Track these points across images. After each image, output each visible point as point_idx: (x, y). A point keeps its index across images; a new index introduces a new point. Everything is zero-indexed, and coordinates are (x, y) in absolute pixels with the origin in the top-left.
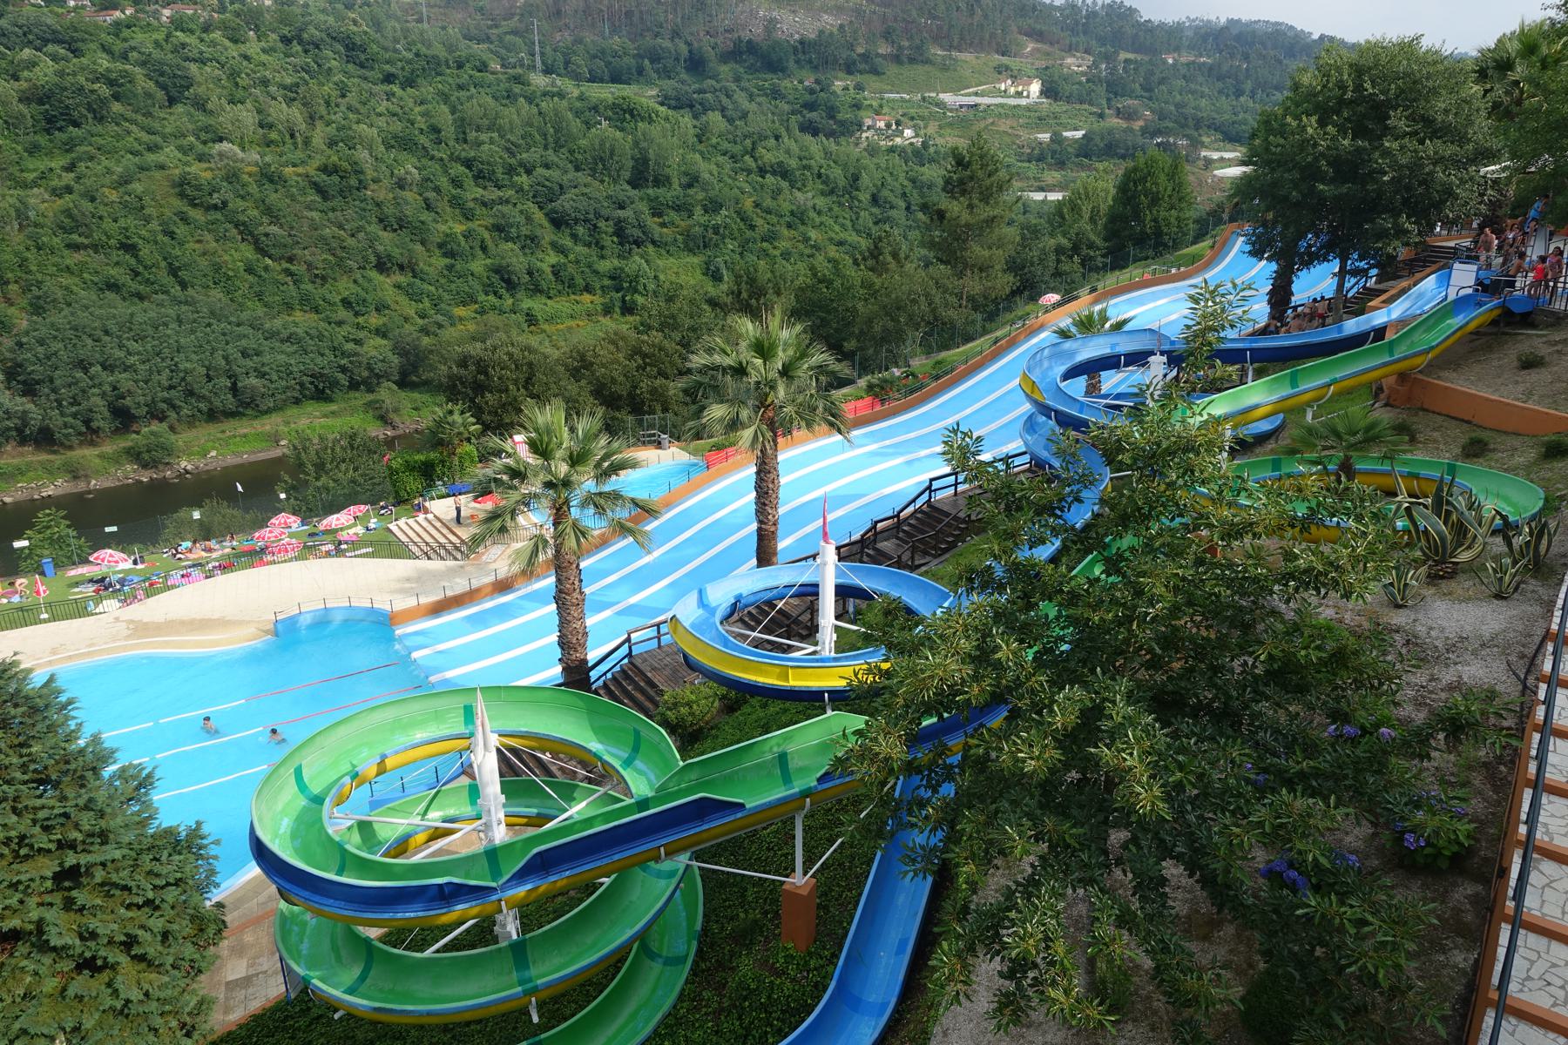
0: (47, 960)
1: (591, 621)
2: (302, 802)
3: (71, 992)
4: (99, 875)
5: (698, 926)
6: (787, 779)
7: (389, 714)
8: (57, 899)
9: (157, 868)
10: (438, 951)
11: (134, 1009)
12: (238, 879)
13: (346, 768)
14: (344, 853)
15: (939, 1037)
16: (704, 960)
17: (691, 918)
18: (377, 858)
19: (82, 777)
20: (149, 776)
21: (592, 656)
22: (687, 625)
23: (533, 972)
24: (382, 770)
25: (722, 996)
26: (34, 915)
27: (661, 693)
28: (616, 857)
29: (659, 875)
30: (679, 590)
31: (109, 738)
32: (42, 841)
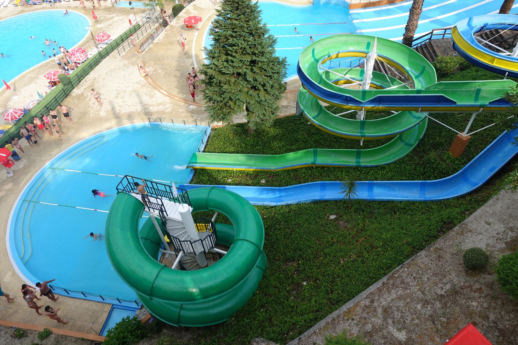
0: (246, 83)
1: (420, 22)
2: (313, 60)
3: (249, 93)
4: (260, 65)
5: (421, 137)
6: (476, 99)
7: (344, 38)
8: (249, 67)
9: (273, 67)
10: (340, 116)
11: (262, 103)
12: (292, 78)
13: (327, 53)
14: (321, 78)
15: (494, 200)
16: (418, 148)
17: (419, 134)
18: (330, 83)
19: (260, 35)
20: (275, 40)
21: (416, 36)
22: (459, 31)
23: (365, 131)
24: (337, 57)
25: (420, 160)
26: (245, 70)
27: (436, 56)
28: (404, 106)
29: (414, 117)
30: (459, 17)
31: (268, 26)
32: (249, 51)
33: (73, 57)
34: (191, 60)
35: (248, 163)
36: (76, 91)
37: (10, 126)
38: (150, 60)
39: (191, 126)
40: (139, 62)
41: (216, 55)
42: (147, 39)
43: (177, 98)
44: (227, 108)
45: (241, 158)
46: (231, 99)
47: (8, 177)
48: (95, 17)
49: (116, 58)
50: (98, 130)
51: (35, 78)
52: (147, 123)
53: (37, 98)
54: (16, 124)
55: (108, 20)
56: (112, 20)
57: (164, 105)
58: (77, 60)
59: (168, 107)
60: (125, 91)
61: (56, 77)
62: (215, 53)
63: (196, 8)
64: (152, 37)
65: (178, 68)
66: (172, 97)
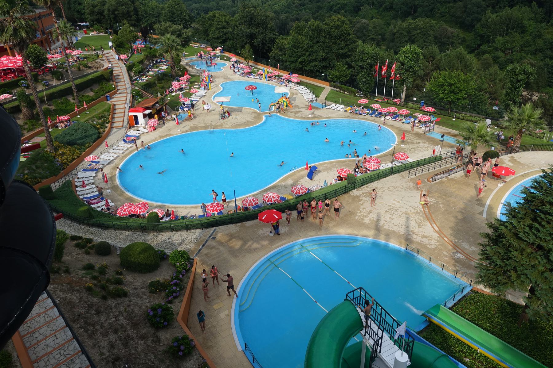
3: (545, 274)
33: (367, 163)
34: (481, 209)
35: (502, 354)
36: (355, 192)
37: (291, 197)
38: (436, 192)
39: (450, 274)
40: (424, 190)
41: (519, 216)
42: (444, 172)
43: (446, 239)
44: (505, 277)
45: (494, 342)
46: (515, 269)
47: (269, 235)
48: (403, 138)
49: (404, 178)
50: (355, 232)
51: (330, 169)
52: (403, 249)
53: (322, 184)
54: (296, 198)
55: (414, 143)
56: (417, 145)
57: (429, 240)
58: (369, 167)
59: (433, 243)
60: (397, 210)
61: (346, 174)
62: (519, 213)
63: (513, 160)
64: (449, 171)
65: (463, 211)
66: (442, 235)
